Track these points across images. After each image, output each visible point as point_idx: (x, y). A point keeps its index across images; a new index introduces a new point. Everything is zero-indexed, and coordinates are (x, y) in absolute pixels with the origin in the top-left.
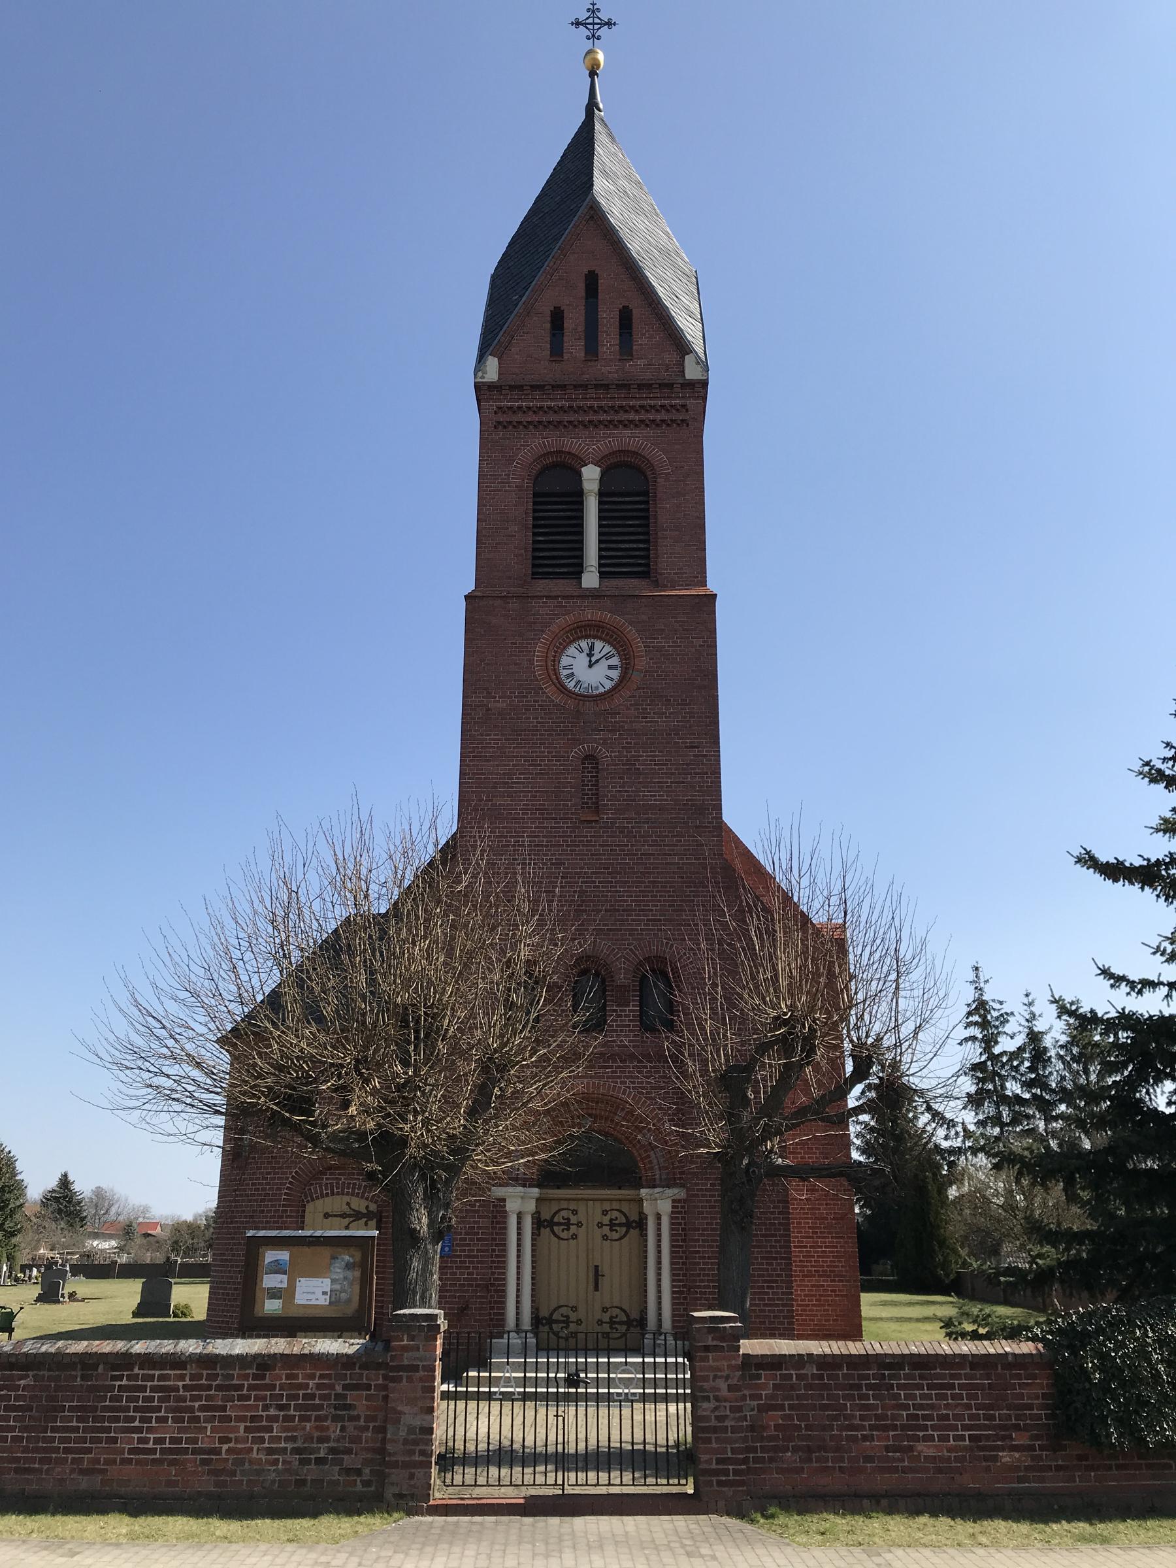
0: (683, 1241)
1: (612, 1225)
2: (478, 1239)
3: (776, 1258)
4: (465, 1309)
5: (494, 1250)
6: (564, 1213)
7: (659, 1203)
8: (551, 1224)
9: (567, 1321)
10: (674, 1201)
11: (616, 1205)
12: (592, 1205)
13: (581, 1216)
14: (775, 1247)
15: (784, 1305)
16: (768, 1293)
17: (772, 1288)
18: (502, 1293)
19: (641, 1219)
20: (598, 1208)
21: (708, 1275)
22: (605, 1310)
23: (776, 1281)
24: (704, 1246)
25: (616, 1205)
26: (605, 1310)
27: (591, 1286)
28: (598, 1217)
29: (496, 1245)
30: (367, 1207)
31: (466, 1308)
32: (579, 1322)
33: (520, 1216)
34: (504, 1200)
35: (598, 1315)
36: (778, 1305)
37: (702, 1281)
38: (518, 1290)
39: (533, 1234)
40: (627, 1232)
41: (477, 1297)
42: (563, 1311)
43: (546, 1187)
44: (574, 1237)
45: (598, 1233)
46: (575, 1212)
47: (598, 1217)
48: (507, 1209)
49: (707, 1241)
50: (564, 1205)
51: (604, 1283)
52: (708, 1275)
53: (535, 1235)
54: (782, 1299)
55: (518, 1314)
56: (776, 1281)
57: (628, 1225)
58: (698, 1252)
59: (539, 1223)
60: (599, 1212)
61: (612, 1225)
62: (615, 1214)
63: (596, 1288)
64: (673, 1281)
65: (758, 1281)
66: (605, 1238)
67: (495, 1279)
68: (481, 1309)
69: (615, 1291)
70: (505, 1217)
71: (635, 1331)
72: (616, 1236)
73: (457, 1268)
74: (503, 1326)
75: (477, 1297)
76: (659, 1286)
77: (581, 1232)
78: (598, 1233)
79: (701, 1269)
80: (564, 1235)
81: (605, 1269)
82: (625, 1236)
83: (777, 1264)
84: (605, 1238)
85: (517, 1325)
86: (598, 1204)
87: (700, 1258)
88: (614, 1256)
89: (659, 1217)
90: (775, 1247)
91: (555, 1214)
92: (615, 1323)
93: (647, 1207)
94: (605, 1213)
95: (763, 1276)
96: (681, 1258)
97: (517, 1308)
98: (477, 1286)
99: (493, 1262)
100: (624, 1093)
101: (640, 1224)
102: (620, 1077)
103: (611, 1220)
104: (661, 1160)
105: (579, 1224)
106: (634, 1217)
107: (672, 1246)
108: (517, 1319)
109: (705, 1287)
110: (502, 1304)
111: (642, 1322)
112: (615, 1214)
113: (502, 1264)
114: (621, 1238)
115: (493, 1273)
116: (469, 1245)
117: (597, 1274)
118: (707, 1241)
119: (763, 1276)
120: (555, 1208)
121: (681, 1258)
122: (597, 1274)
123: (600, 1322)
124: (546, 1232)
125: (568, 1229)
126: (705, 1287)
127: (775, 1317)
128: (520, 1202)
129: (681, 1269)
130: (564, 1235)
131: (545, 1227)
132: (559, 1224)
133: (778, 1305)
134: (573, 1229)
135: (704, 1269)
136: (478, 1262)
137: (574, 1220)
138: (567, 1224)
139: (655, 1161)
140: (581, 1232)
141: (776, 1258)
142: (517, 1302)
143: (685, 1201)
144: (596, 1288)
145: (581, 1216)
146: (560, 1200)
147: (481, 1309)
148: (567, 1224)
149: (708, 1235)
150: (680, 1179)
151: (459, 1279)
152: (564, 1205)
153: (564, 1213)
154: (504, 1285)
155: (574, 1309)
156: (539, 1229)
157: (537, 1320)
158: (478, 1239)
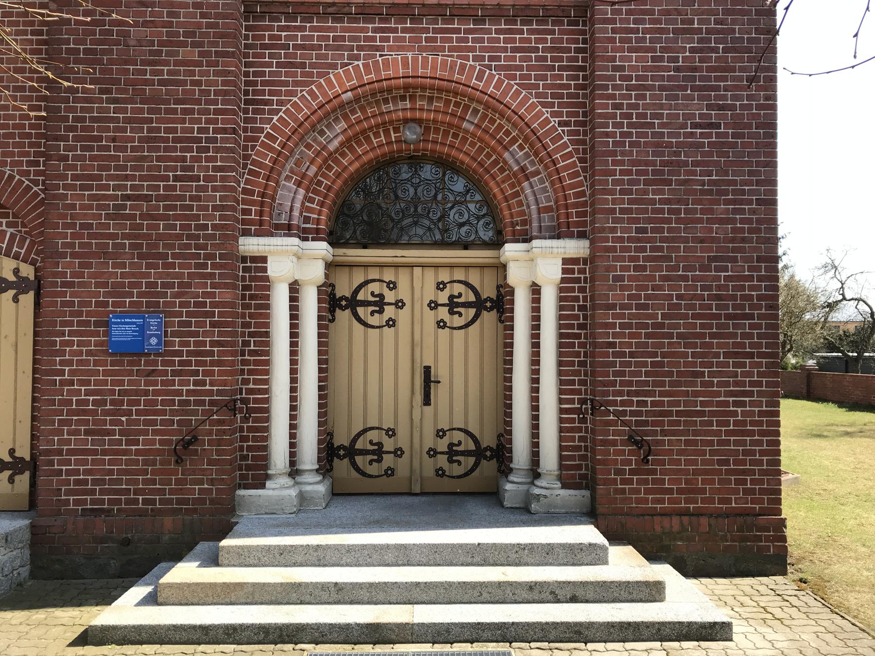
0: (581, 327)
1: (453, 305)
2: (213, 325)
3: (751, 355)
4: (190, 443)
5: (246, 344)
6: (375, 287)
7: (538, 266)
8: (353, 303)
9: (379, 452)
10: (565, 261)
11: (459, 275)
12: (417, 276)
13: (403, 293)
14: (750, 336)
15: (762, 433)
16: (735, 414)
17: (742, 404)
18: (264, 412)
19: (500, 296)
20: (430, 278)
21: (630, 384)
22: (440, 433)
23: (750, 394)
24: (623, 335)
25: (459, 275)
26: (440, 433)
27: (419, 397)
28: (430, 293)
29: (251, 335)
30: (16, 271)
31: (194, 440)
32: (398, 452)
33: (294, 289)
34: (264, 259)
35: (429, 441)
36: (751, 433)
37: (620, 393)
38: (293, 408)
39: (320, 318)
40: (476, 317)
41: (213, 423)
42: (373, 435)
43: (346, 245)
44: (391, 323)
45: (430, 317)
46: (392, 286)
47: (430, 293)
48: (270, 273)
49: (629, 326)
50: (373, 274)
51: (440, 394)
52: (630, 384)
53: (326, 320)
54: (760, 423)
55: (292, 445)
56: (750, 394)
57: (479, 305)
58: (612, 345)
59: (332, 303)
60: (430, 286)
61: (453, 305)
62: (458, 288)
63: (427, 401)
64: (561, 392)
65: (718, 394)
66: (441, 324)
67: (250, 391)
68: (219, 442)
69: (460, 403)
70: (268, 288)
71: (343, 290)
72: (458, 321)
73: (175, 373)
74: (266, 467)
75: (213, 423)
76: (294, 317)
77: (403, 316)
78: (430, 317)
79: (616, 374)
80: (375, 320)
81: (441, 372)
82: (473, 321)
83: (753, 365)
84: (441, 324)
85: (292, 463)
86: (430, 274)
87: (615, 354)
88: (457, 355)
89: (536, 290)
90: (750, 336)
91: (472, 470)
92: (458, 453)
93: (517, 277)
94: (441, 286)
95: (727, 384)
96: (578, 354)
97: (292, 436)
98: (212, 403)
99: (244, 362)
100: (480, 78)
101: (501, 303)
102: (472, 49)
103: (451, 297)
104: (542, 197)
105: (399, 304)
106: (489, 292)
107: (561, 336)
108: (292, 455)
109: (623, 403)
110: (263, 430)
111: (501, 452)
112: (458, 288)
113: (264, 366)
114: (467, 326)
115: (246, 382)
116: (196, 334)
117: (428, 379)
118: (629, 326)
119: (727, 384)
120: (359, 277)
121: (578, 354)
122: (428, 379)
123: (433, 453)
124: (344, 316)
125: (381, 312)
126: (623, 403)
127: (746, 453)
128: (294, 264)
129: (577, 373)
130: (375, 320)
131: (343, 308)
132: (365, 303)
133: (751, 433)
134: (389, 312)
135: (622, 374)
136: (213, 363)
137: (390, 297)
138: (380, 304)
139: (531, 198)
140: (403, 316)
141: (751, 355)
142: (291, 422)
143: (585, 261)
144: (427, 401)
145: (403, 293)
146: (366, 266)
147: (219, 442)
148: (380, 304)
149: (631, 317)
150: (578, 224)
151: (179, 393)
152: (373, 274)
153: (375, 287)
154: (267, 401)
155: (391, 433)
156: (332, 311)
157: (330, 452)
158: (213, 325)
